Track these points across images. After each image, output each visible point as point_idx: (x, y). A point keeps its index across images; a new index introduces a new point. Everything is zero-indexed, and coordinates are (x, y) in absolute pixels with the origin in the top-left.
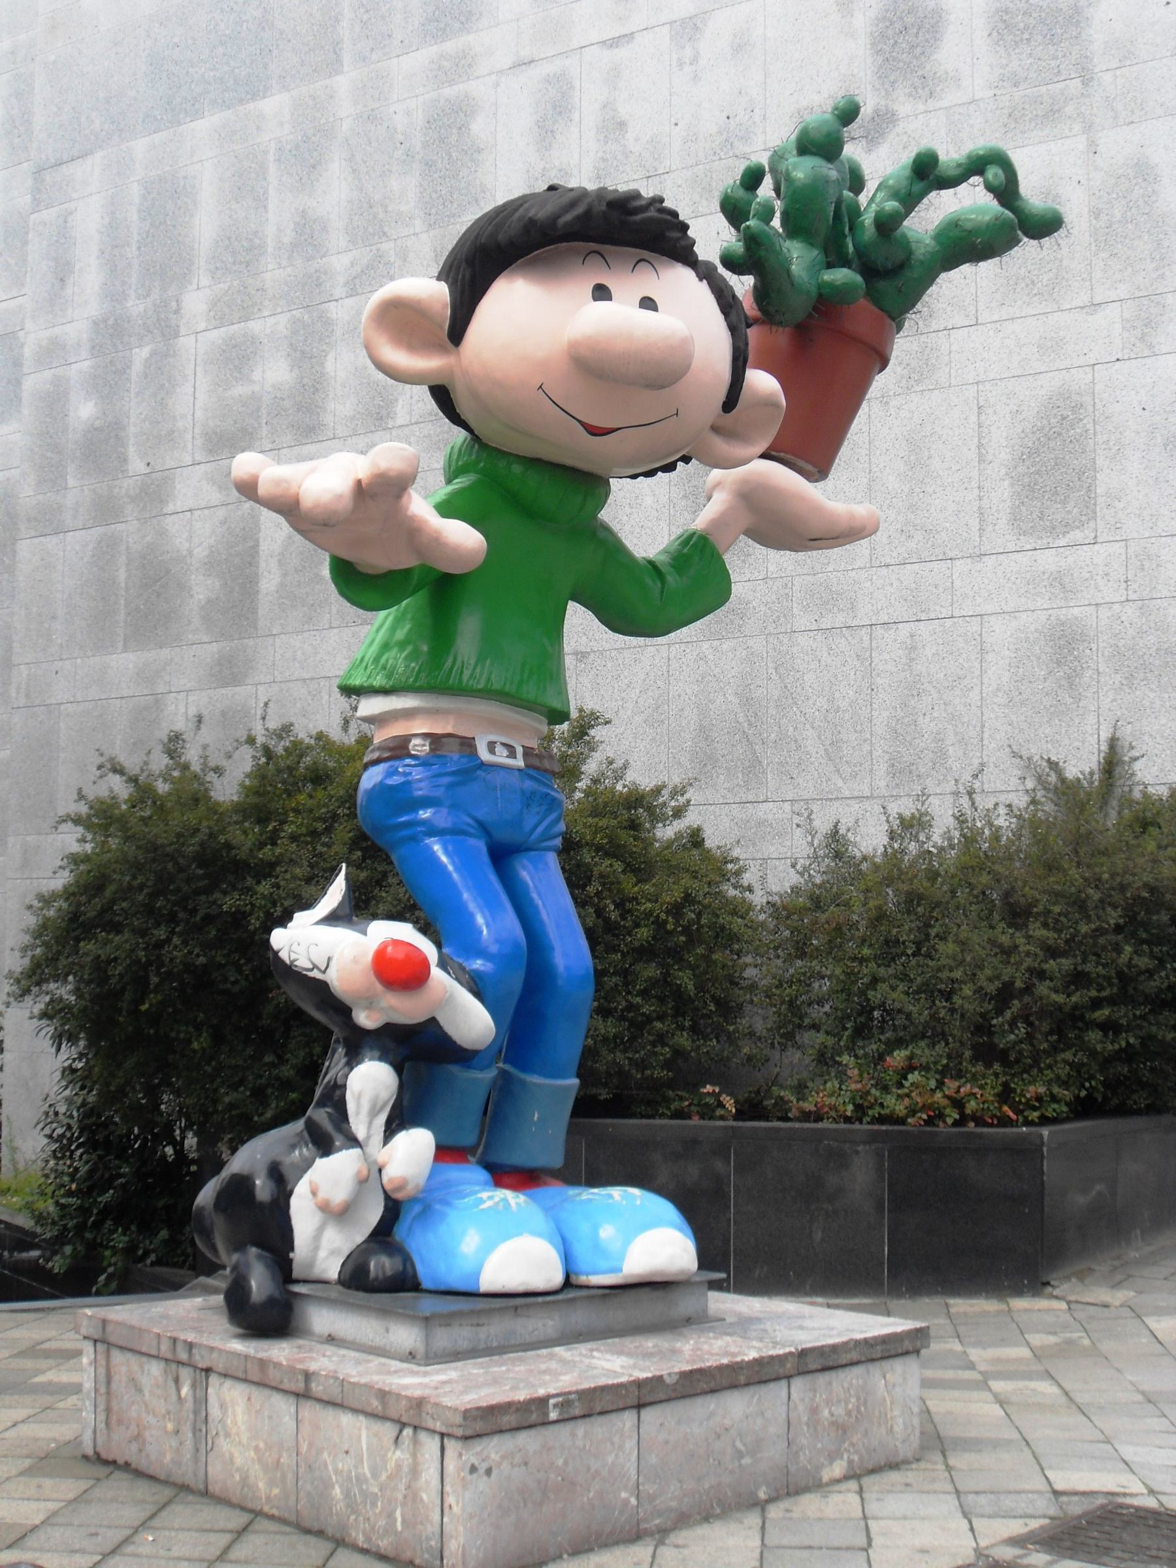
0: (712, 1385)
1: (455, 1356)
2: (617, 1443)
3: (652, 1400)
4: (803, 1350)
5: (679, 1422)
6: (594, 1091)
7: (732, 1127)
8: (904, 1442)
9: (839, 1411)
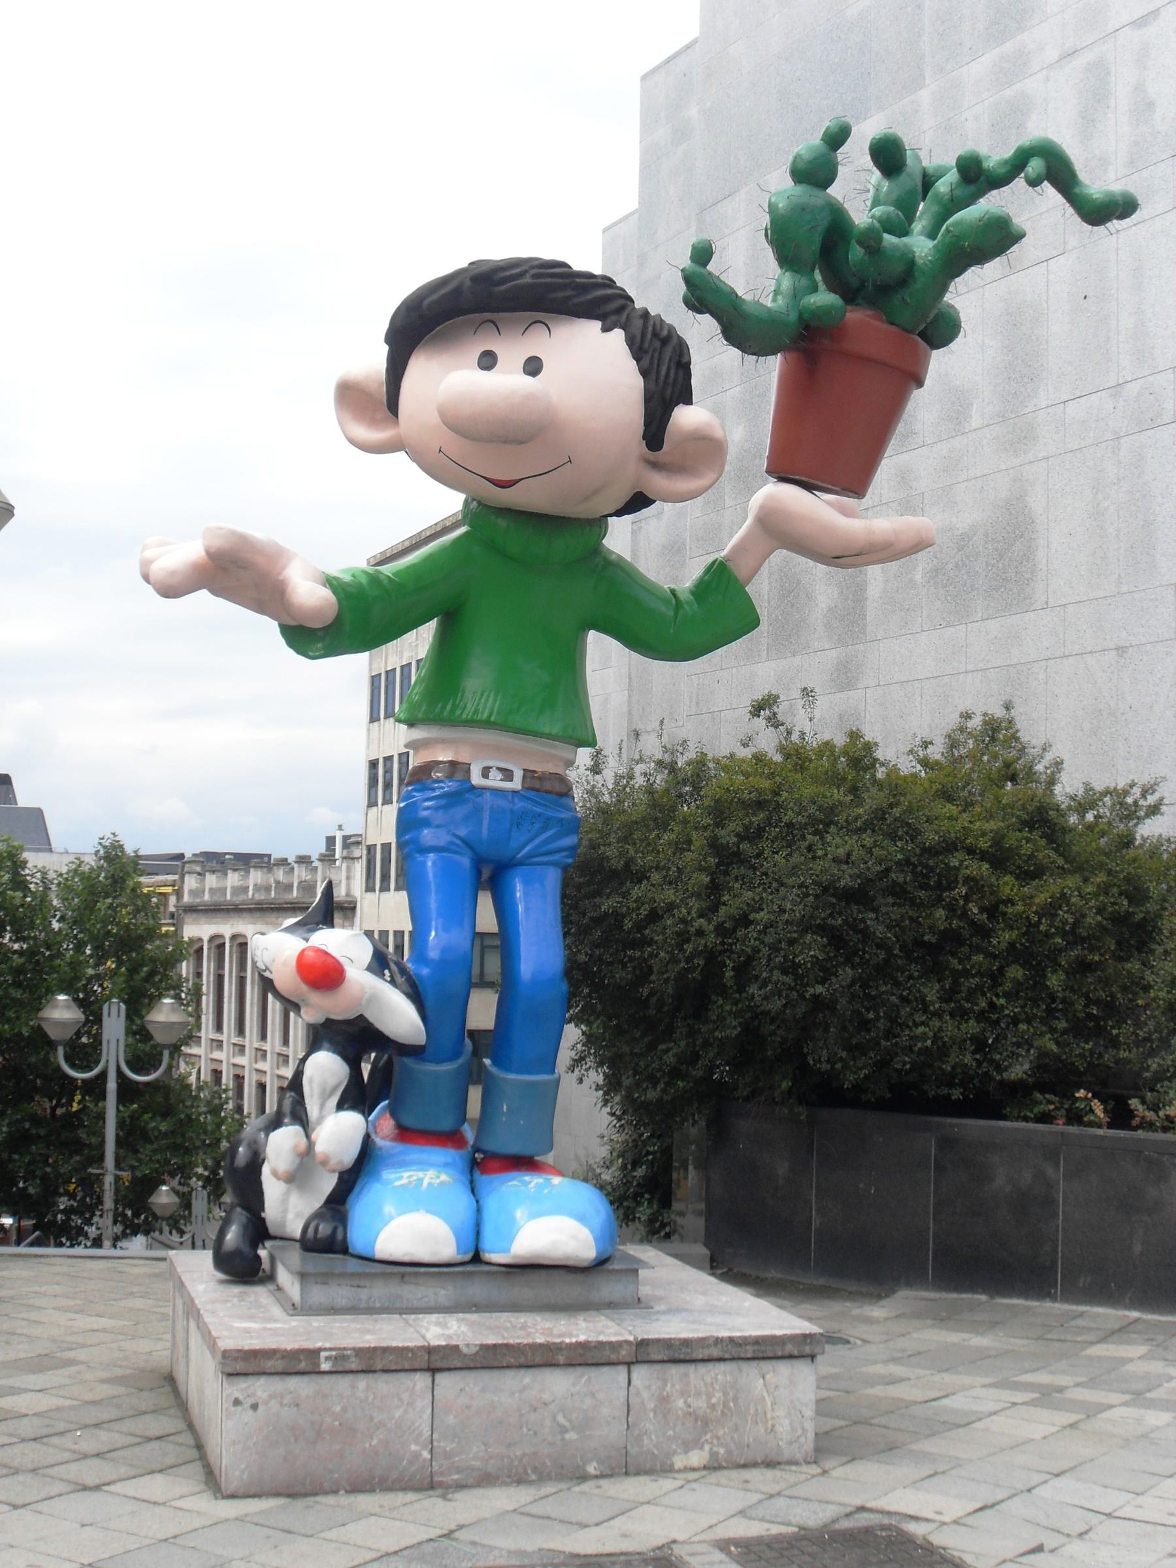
0: (522, 1360)
1: (332, 1310)
2: (408, 1401)
3: (446, 1365)
4: (643, 1341)
5: (483, 1390)
6: (946, 1091)
7: (1062, 1134)
8: (790, 1443)
9: (700, 1404)
